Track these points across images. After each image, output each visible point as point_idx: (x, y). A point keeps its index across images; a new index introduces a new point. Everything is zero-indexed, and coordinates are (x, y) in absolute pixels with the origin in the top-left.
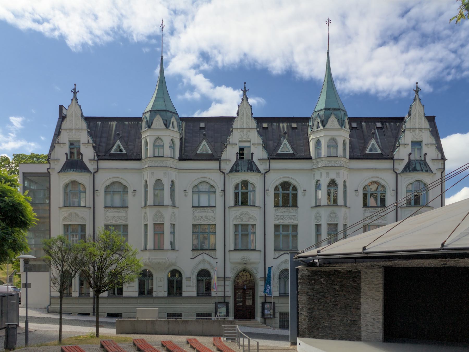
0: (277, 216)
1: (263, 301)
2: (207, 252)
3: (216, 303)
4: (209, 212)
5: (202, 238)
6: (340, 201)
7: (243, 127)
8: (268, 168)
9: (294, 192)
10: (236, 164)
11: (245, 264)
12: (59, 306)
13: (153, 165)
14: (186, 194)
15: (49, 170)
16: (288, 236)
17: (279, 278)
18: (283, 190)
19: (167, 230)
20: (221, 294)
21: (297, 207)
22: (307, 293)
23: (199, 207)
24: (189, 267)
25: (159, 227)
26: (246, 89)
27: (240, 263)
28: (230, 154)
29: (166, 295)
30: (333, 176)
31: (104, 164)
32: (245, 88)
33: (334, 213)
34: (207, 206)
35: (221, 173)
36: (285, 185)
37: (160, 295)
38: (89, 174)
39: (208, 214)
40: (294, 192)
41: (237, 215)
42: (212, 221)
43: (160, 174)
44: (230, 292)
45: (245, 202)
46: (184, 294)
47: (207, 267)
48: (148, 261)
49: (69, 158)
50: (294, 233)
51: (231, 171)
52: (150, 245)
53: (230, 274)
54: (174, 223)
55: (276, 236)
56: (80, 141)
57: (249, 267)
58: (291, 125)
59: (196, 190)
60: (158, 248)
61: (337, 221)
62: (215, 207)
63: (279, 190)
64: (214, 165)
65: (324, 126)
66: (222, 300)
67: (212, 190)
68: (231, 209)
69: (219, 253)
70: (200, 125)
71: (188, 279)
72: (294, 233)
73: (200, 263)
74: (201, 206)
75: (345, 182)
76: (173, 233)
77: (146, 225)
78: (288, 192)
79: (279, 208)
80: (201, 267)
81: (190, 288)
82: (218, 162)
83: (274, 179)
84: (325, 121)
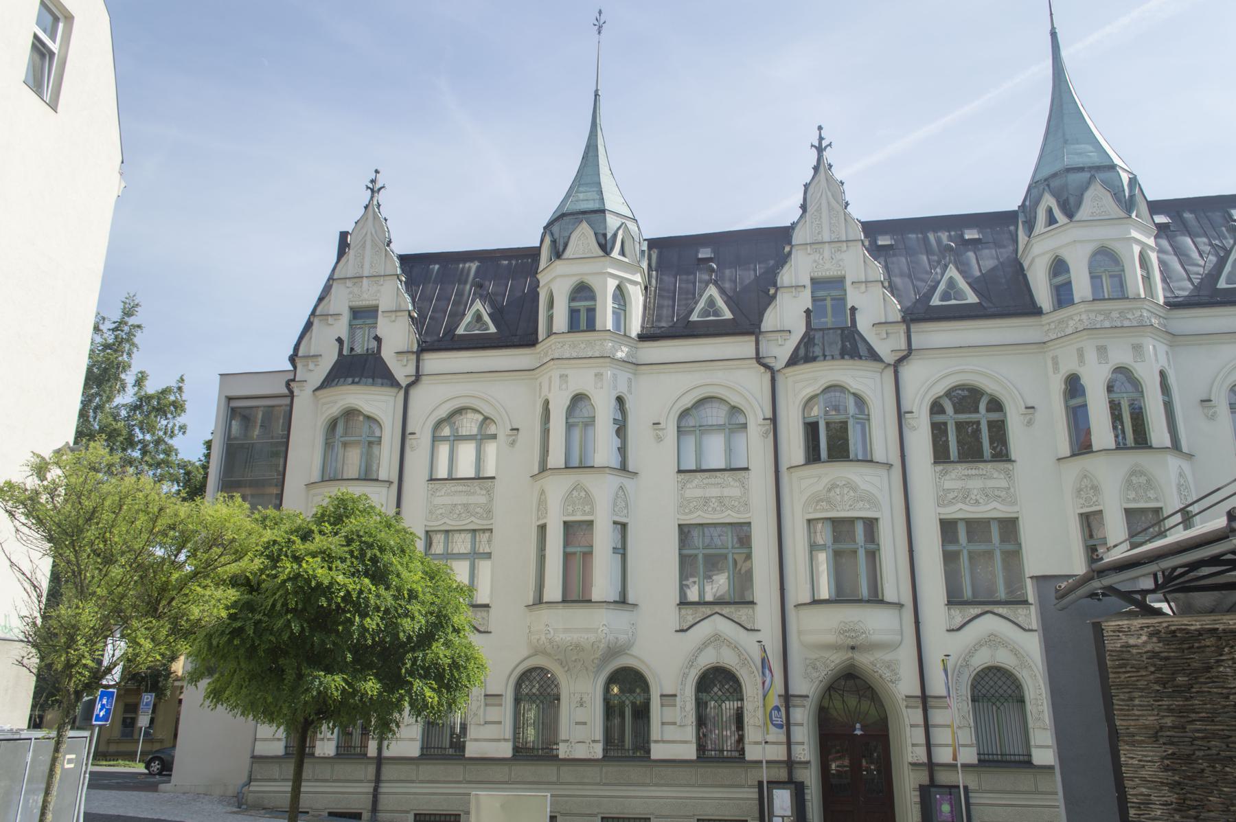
0: (941, 493)
1: (924, 778)
2: (726, 610)
3: (760, 784)
4: (730, 488)
5: (709, 551)
6: (1158, 433)
7: (819, 239)
8: (903, 345)
9: (994, 416)
10: (807, 340)
11: (853, 648)
12: (287, 787)
13: (567, 355)
14: (660, 433)
15: (292, 384)
16: (989, 554)
17: (973, 701)
18: (956, 412)
19: (603, 539)
20: (779, 753)
21: (1010, 460)
22: (1156, 735)
23: (700, 471)
24: (669, 659)
25: (576, 531)
26: (824, 144)
27: (836, 647)
28: (788, 314)
29: (599, 753)
30: (1121, 355)
31: (435, 362)
32: (821, 139)
33: (1142, 473)
34: (723, 467)
35: (762, 369)
36: (967, 397)
37: (580, 752)
38: (394, 390)
39: (727, 492)
40: (994, 416)
41: (816, 489)
42: (738, 512)
43: (581, 379)
44: (806, 749)
45: (840, 451)
46: (657, 752)
47: (728, 659)
48: (543, 638)
49: (345, 352)
50: (1010, 547)
51: (793, 361)
52: (553, 590)
53: (806, 685)
54: (624, 520)
55: (950, 558)
56: (377, 307)
57: (864, 660)
58: (962, 236)
59: (689, 421)
60: (576, 594)
61: (1157, 500)
62: (747, 469)
63: (943, 411)
64: (742, 347)
65: (1070, 215)
66: (782, 774)
67: (735, 421)
68: (798, 473)
69: (765, 612)
70: (697, 252)
71: (669, 698)
72: (1010, 547)
73: (705, 645)
74: (704, 467)
75: (1162, 374)
76: (622, 551)
77: (542, 528)
78: (973, 417)
79: (949, 467)
80: (708, 659)
81: (673, 735)
82: (753, 338)
83: (925, 381)
84: (1072, 200)
